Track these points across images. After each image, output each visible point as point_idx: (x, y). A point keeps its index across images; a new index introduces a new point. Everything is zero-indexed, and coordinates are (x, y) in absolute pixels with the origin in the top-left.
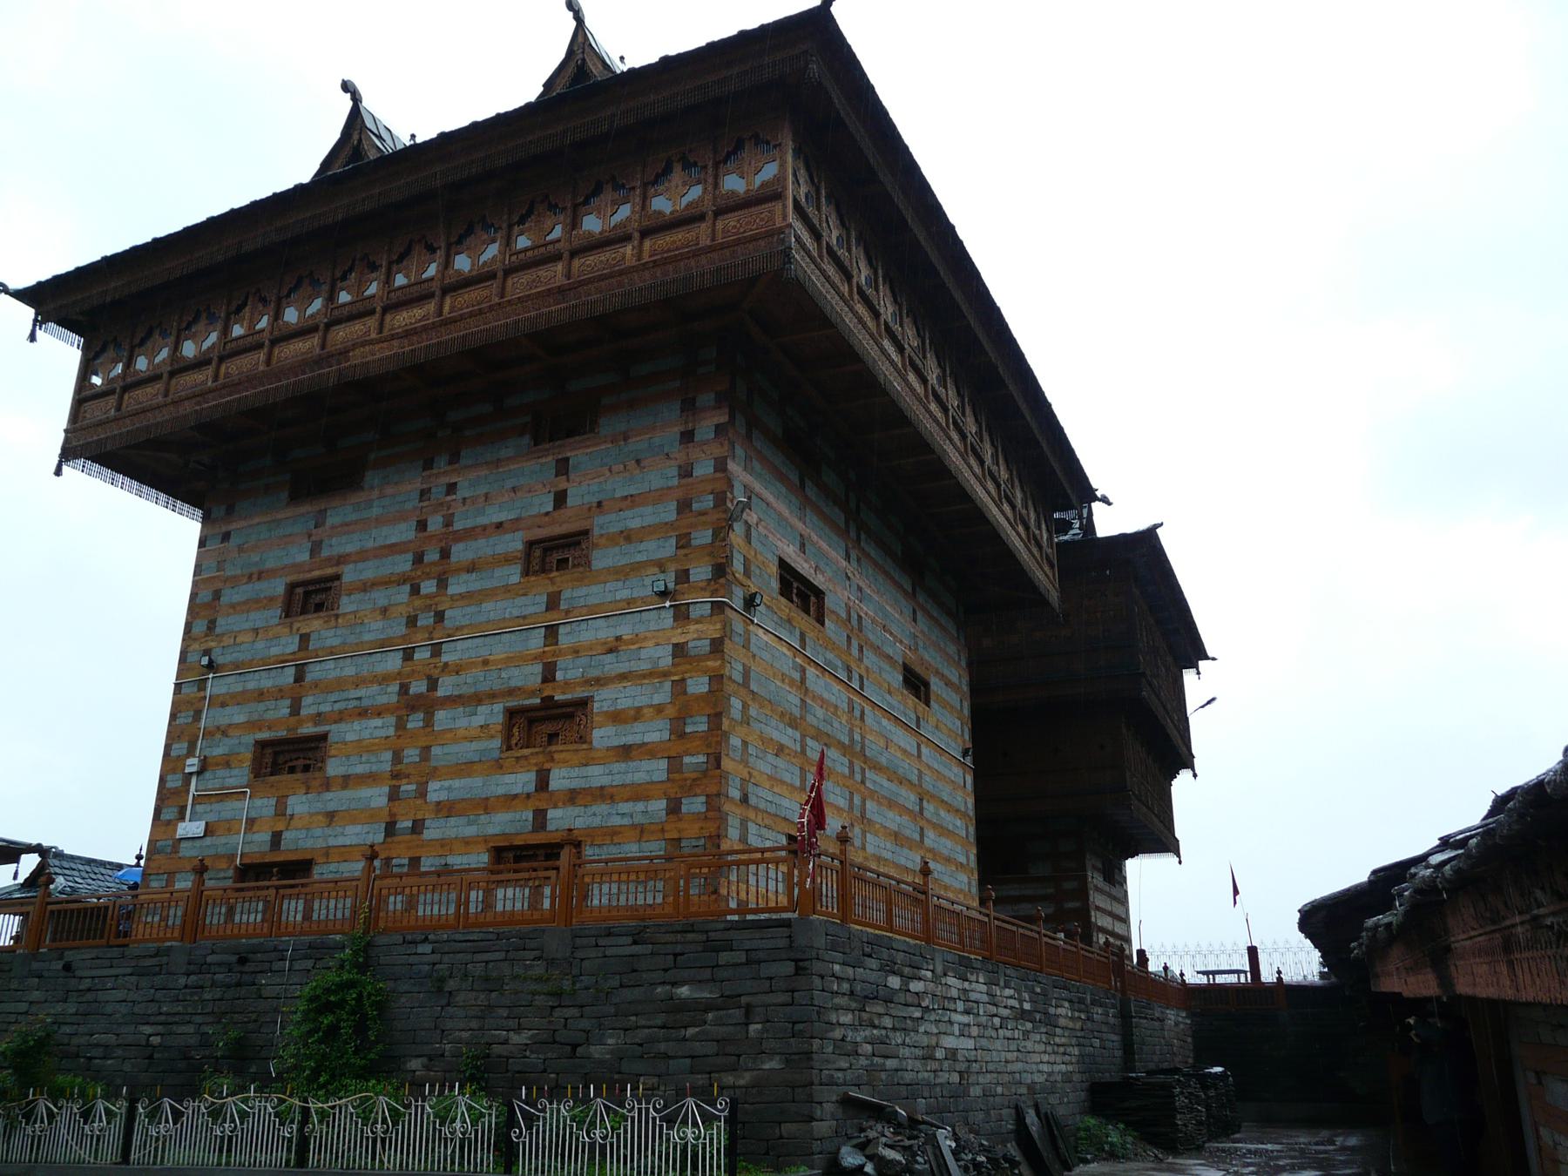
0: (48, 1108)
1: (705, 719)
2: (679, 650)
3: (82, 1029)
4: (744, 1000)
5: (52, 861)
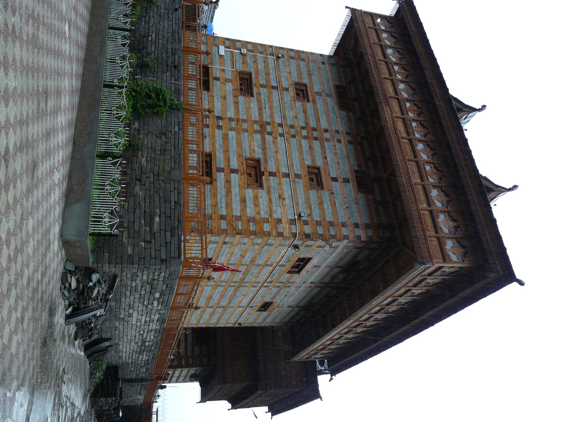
1: (254, 229)
2: (279, 221)
3: (155, 14)
4: (153, 240)
5: (213, 5)
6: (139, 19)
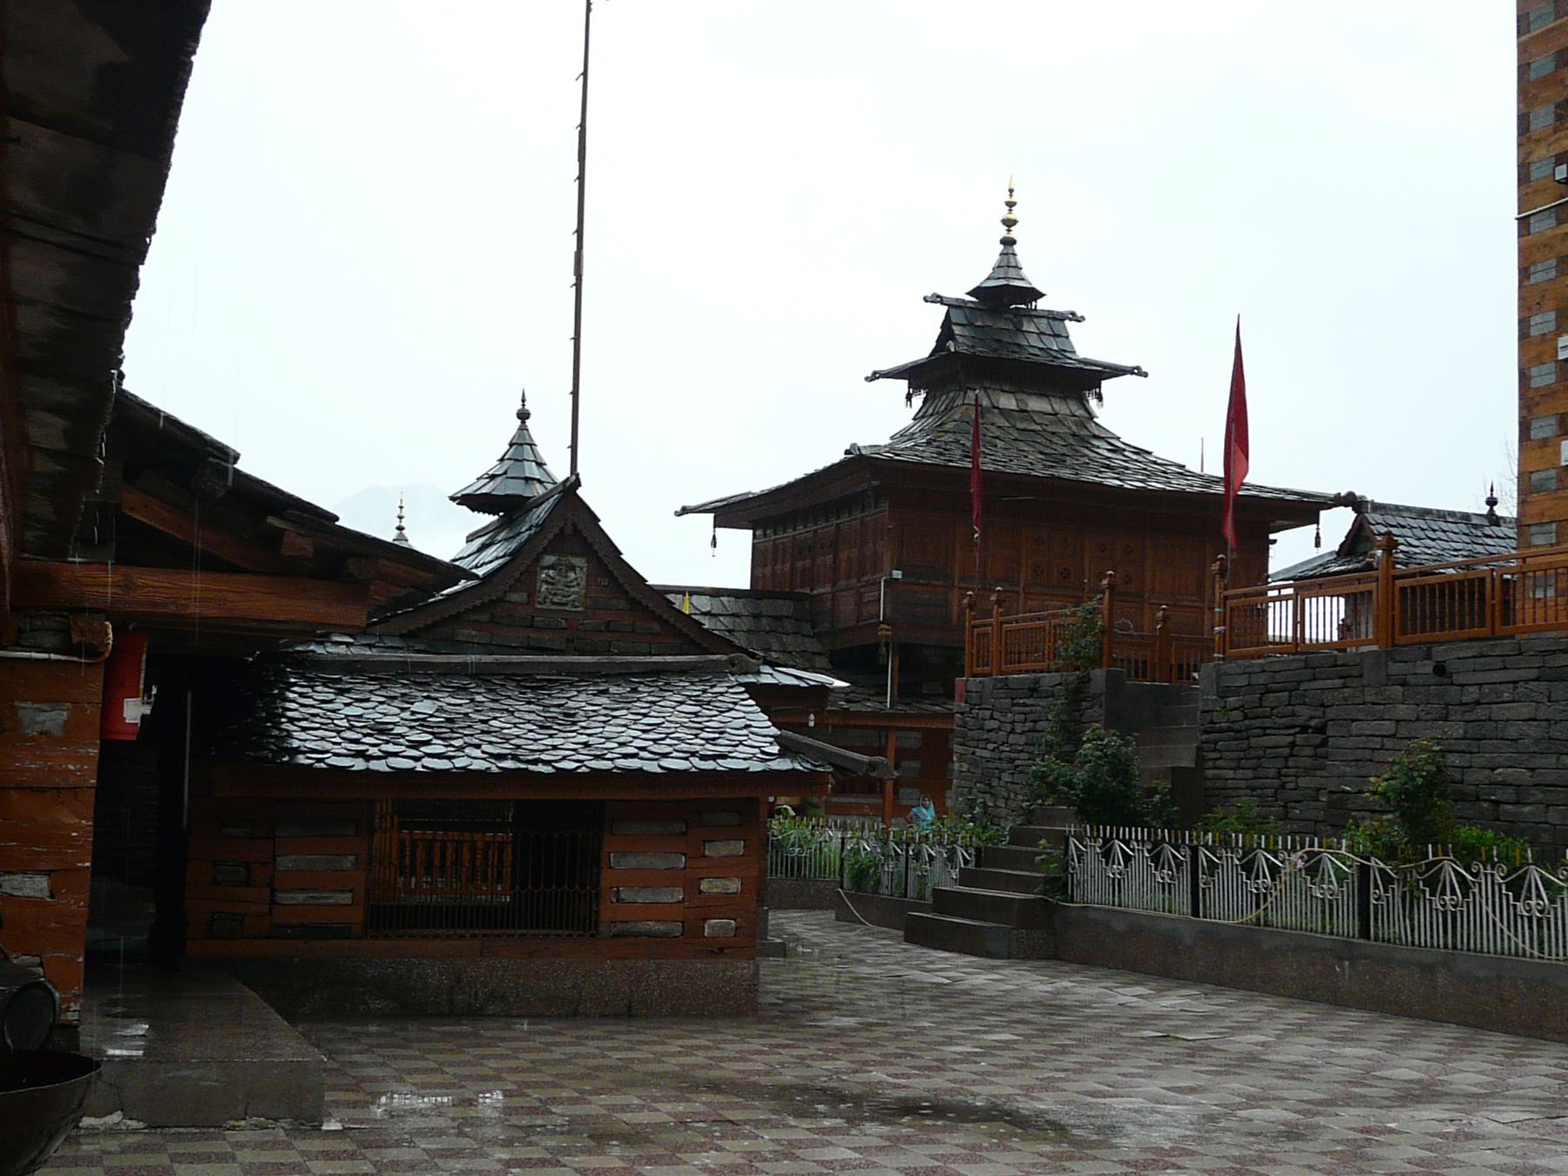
0: (1457, 874)
3: (1478, 760)
5: (1372, 517)
6: (1512, 828)
